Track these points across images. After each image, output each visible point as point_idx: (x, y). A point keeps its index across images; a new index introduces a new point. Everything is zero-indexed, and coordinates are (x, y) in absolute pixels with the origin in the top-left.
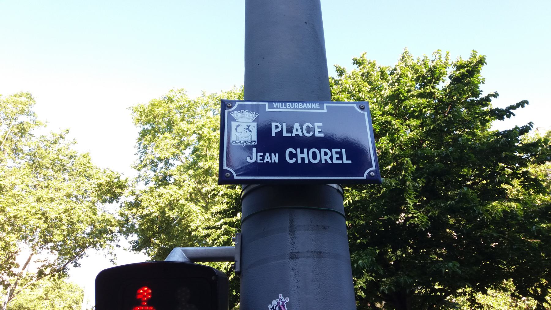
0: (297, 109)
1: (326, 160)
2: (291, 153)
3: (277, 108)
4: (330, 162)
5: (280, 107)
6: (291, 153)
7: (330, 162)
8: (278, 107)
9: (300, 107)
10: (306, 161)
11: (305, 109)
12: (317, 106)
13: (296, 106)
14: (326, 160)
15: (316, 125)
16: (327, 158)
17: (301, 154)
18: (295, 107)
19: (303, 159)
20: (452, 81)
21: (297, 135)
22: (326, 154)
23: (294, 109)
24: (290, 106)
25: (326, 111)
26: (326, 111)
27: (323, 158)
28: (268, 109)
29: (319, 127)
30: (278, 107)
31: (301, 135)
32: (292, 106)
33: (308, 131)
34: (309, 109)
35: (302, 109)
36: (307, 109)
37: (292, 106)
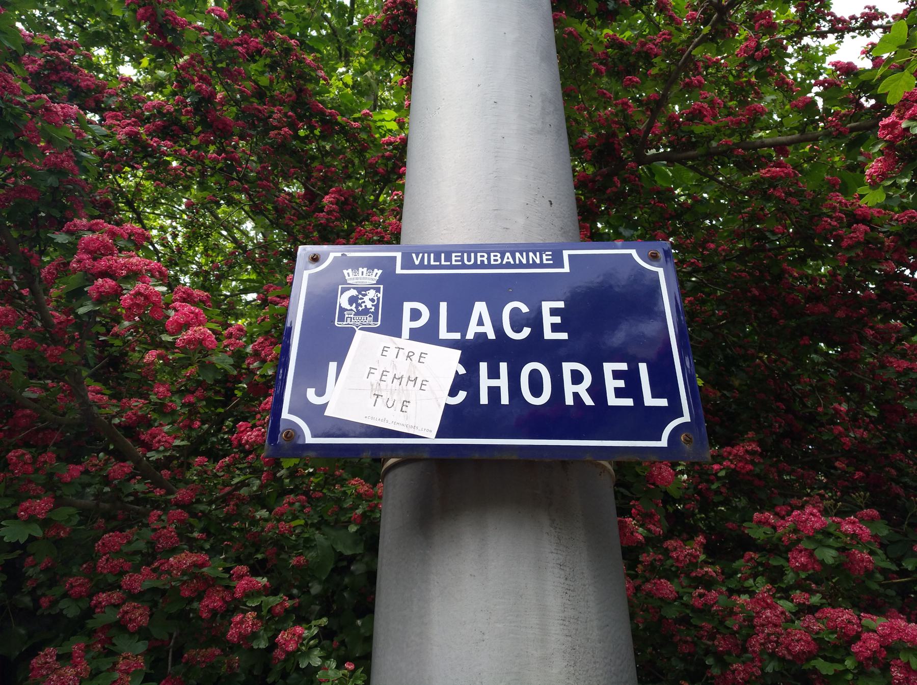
0: (482, 266)
1: (576, 396)
2: (515, 312)
3: (421, 266)
4: (588, 401)
5: (432, 263)
6: (515, 312)
7: (588, 401)
8: (426, 263)
9: (492, 262)
10: (505, 399)
11: (509, 265)
12: (544, 257)
13: (479, 259)
14: (576, 396)
15: (546, 306)
16: (582, 389)
17: (489, 378)
18: (479, 263)
19: (494, 392)
20: (290, 473)
21: (481, 336)
22: (577, 378)
23: (475, 266)
24: (462, 260)
25: (543, 303)
26: (543, 303)
27: (569, 389)
28: (399, 271)
29: (554, 312)
30: (426, 263)
31: (491, 336)
32: (469, 260)
33: (518, 322)
34: (521, 266)
35: (500, 266)
36: (515, 266)
37: (469, 260)
